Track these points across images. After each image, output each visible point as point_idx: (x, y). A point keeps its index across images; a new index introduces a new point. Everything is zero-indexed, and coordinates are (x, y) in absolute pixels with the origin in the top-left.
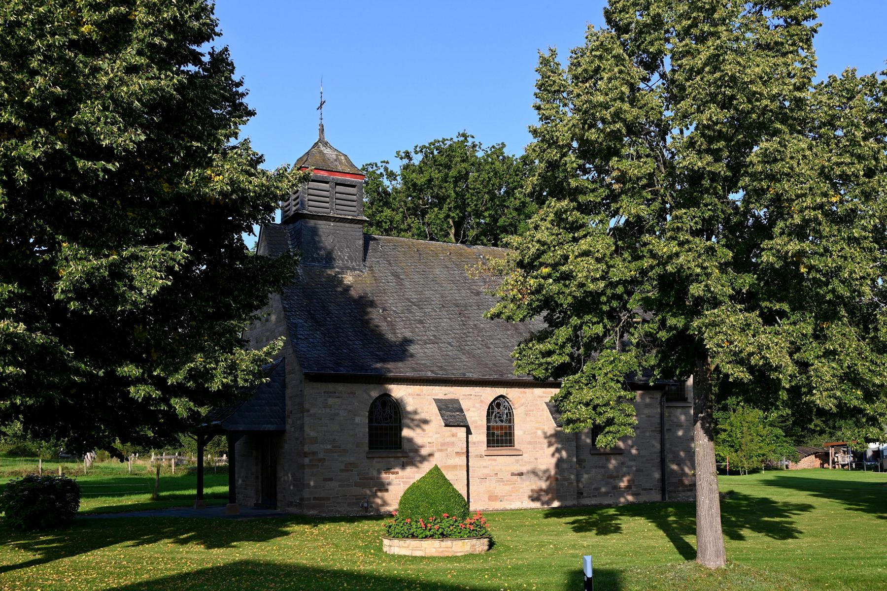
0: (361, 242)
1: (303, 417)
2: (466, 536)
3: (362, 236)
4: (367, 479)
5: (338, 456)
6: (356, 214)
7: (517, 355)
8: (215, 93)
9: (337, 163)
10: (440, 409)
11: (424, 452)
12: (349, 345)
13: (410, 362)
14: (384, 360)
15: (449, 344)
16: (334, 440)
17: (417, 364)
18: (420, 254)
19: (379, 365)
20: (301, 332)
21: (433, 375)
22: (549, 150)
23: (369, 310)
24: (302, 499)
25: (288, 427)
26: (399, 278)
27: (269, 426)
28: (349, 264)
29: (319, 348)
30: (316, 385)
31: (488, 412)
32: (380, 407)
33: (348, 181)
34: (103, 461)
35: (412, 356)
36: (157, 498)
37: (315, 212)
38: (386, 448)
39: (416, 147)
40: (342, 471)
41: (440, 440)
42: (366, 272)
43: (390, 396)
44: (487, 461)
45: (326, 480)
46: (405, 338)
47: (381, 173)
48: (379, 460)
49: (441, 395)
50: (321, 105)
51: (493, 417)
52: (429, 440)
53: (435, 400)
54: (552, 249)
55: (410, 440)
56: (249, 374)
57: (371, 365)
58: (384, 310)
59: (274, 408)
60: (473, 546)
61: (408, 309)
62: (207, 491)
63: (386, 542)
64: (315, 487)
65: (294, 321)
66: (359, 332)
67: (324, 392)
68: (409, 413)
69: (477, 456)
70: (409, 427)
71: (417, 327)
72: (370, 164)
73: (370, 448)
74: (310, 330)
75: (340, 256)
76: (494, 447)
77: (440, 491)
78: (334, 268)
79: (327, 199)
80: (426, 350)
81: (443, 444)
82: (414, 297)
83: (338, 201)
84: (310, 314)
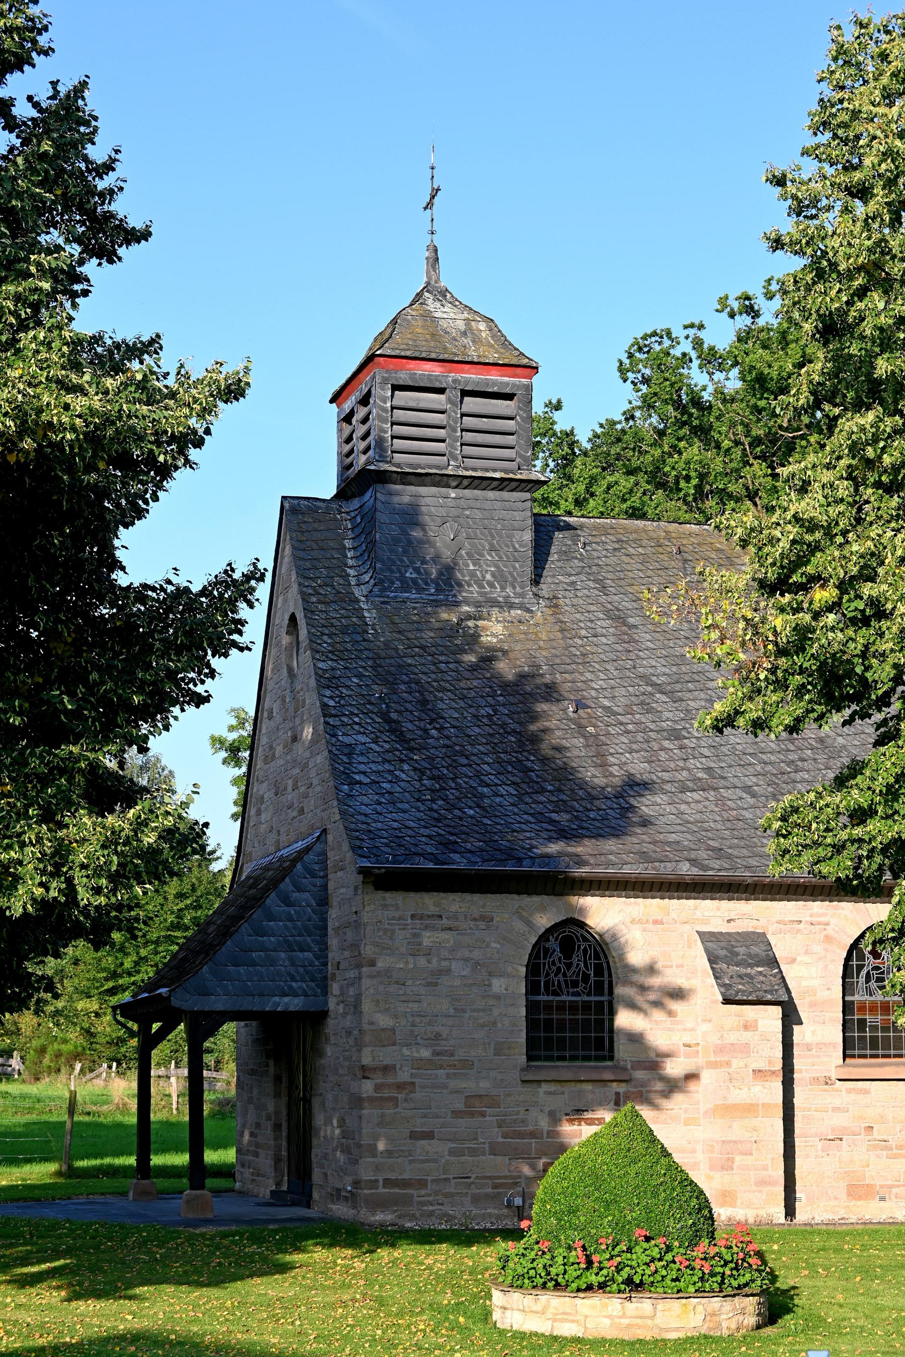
0: (528, 536)
1: (360, 978)
2: (692, 1289)
3: (530, 522)
4: (521, 1135)
5: (448, 1076)
6: (514, 465)
7: (777, 825)
8: (19, 196)
9: (467, 341)
10: (713, 960)
11: (673, 1068)
12: (483, 796)
13: (638, 839)
14: (564, 834)
15: (747, 789)
16: (438, 1036)
17: (654, 843)
18: (685, 561)
19: (553, 848)
20: (362, 767)
21: (695, 871)
22: (820, 287)
23: (542, 707)
24: (357, 1183)
25: (332, 1004)
26: (625, 624)
27: (286, 999)
28: (497, 593)
29: (406, 806)
30: (391, 897)
31: (846, 966)
32: (558, 954)
33: (495, 383)
34: (37, 1079)
35: (645, 823)
36: (71, 1173)
37: (410, 465)
38: (573, 1058)
39: (769, 281)
40: (456, 1114)
41: (714, 1039)
42: (540, 611)
43: (582, 925)
44: (843, 1094)
45: (415, 1136)
46: (630, 775)
47: (684, 355)
48: (552, 1087)
49: (719, 921)
50: (433, 197)
51: (862, 979)
52: (687, 1039)
53: (701, 934)
54: (839, 539)
55: (636, 1038)
56: (99, 876)
57: (532, 847)
58: (580, 705)
59: (300, 955)
60: (713, 1315)
61: (642, 703)
62: (156, 1160)
63: (497, 1297)
64: (389, 1153)
65: (347, 740)
66: (509, 763)
67: (413, 916)
68: (634, 970)
69: (816, 1080)
70: (632, 1006)
71: (663, 749)
72: (654, 334)
73: (530, 1058)
74: (385, 761)
75: (472, 574)
76: (864, 1056)
77: (632, 1171)
78: (457, 604)
79: (441, 433)
80: (683, 807)
81: (720, 1049)
82: (662, 671)
83: (469, 437)
84: (389, 721)
